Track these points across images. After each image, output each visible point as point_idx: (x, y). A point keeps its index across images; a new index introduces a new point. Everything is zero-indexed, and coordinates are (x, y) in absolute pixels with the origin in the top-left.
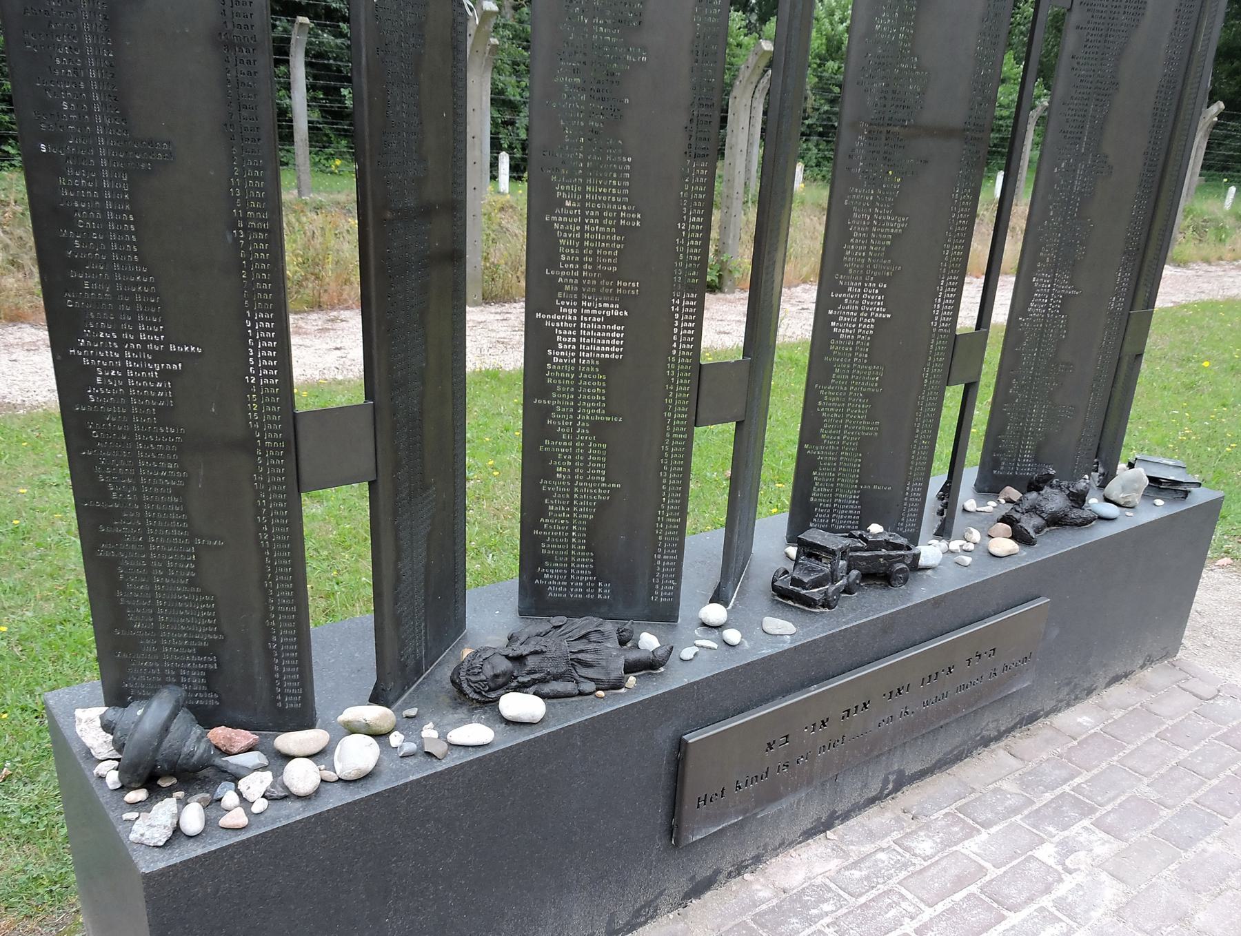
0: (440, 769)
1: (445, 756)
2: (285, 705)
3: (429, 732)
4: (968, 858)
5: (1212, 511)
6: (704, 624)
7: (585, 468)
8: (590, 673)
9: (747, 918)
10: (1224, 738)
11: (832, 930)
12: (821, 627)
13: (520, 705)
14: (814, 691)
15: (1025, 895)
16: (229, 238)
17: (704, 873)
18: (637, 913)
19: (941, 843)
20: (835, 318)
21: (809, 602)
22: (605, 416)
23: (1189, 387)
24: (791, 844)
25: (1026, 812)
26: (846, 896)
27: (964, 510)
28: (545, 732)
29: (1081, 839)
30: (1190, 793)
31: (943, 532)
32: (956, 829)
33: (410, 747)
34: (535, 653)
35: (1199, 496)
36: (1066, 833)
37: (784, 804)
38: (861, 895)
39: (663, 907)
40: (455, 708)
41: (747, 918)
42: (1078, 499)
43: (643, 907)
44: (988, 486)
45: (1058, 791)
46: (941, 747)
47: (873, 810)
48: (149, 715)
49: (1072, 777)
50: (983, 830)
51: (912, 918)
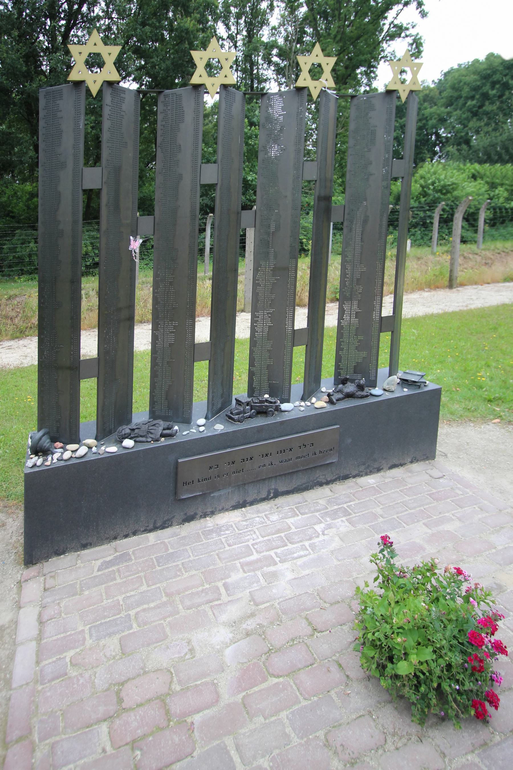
2: (75, 438)
5: (437, 393)
8: (152, 436)
13: (128, 443)
17: (191, 513)
18: (164, 523)
20: (256, 326)
21: (233, 419)
24: (227, 510)
30: (397, 514)
35: (431, 386)
37: (222, 492)
39: (175, 523)
41: (200, 532)
49: (350, 501)
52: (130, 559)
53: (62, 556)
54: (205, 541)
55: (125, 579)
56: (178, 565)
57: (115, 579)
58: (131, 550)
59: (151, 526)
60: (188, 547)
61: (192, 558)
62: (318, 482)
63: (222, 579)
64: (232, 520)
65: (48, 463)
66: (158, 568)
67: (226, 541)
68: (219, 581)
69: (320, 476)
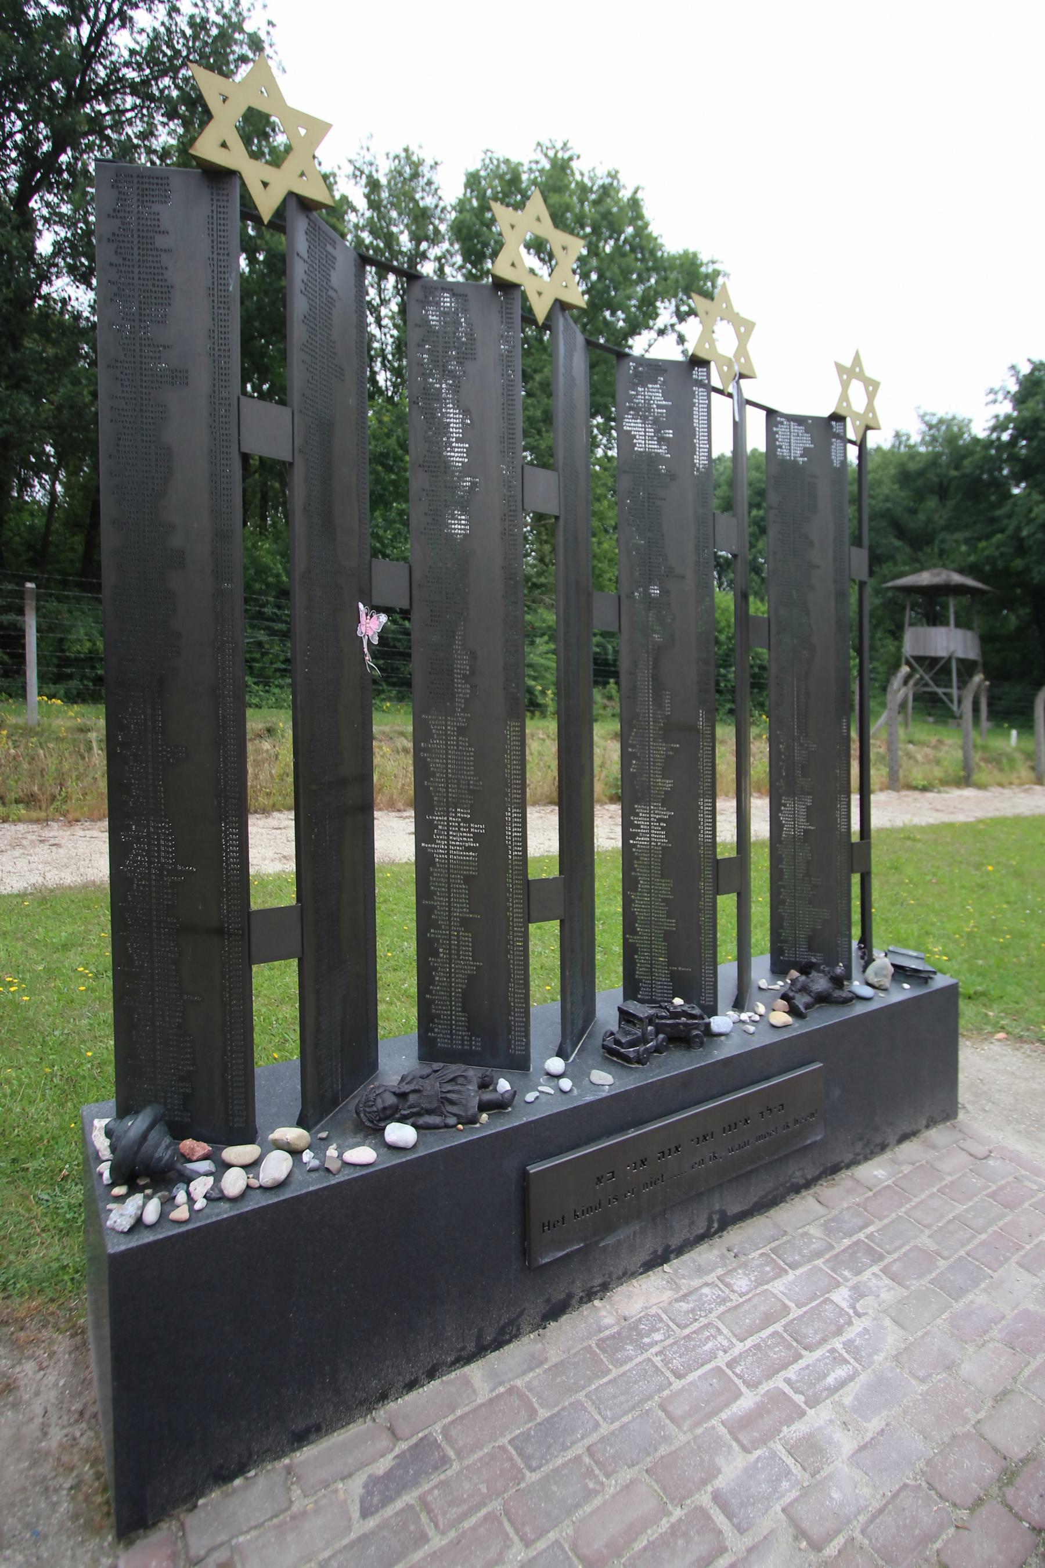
0: (333, 1182)
1: (339, 1172)
3: (332, 1152)
4: (775, 1296)
5: (951, 992)
6: (548, 1074)
7: (458, 950)
9: (593, 1343)
10: (993, 1195)
11: (659, 1358)
12: (633, 1080)
13: (400, 1133)
14: (632, 1133)
15: (818, 1337)
16: (216, 803)
18: (502, 1331)
19: (755, 1281)
20: (635, 846)
21: (626, 1058)
22: (470, 913)
23: (982, 886)
24: (634, 1275)
25: (827, 1256)
26: (674, 1327)
27: (760, 988)
28: (414, 1156)
29: (871, 1284)
30: (963, 1245)
31: (739, 1005)
32: (768, 1269)
33: (315, 1163)
34: (415, 1091)
35: (940, 981)
36: (858, 1278)
37: (622, 1234)
38: (686, 1326)
39: (525, 1328)
40: (355, 1133)
41: (593, 1343)
42: (838, 982)
43: (507, 1325)
44: (779, 969)
45: (855, 1238)
46: (756, 1192)
47: (703, 1248)
48: (135, 1125)
50: (790, 1271)
51: (725, 1352)
52: (445, 1460)
53: (238, 1482)
54: (615, 1372)
55: (453, 1534)
56: (578, 1458)
57: (423, 1538)
58: (438, 1427)
59: (471, 1347)
60: (581, 1396)
61: (605, 1429)
62: (792, 1184)
63: (704, 1482)
64: (653, 1301)
65: (181, 1213)
66: (532, 1477)
67: (666, 1362)
68: (699, 1489)
69: (796, 1172)
